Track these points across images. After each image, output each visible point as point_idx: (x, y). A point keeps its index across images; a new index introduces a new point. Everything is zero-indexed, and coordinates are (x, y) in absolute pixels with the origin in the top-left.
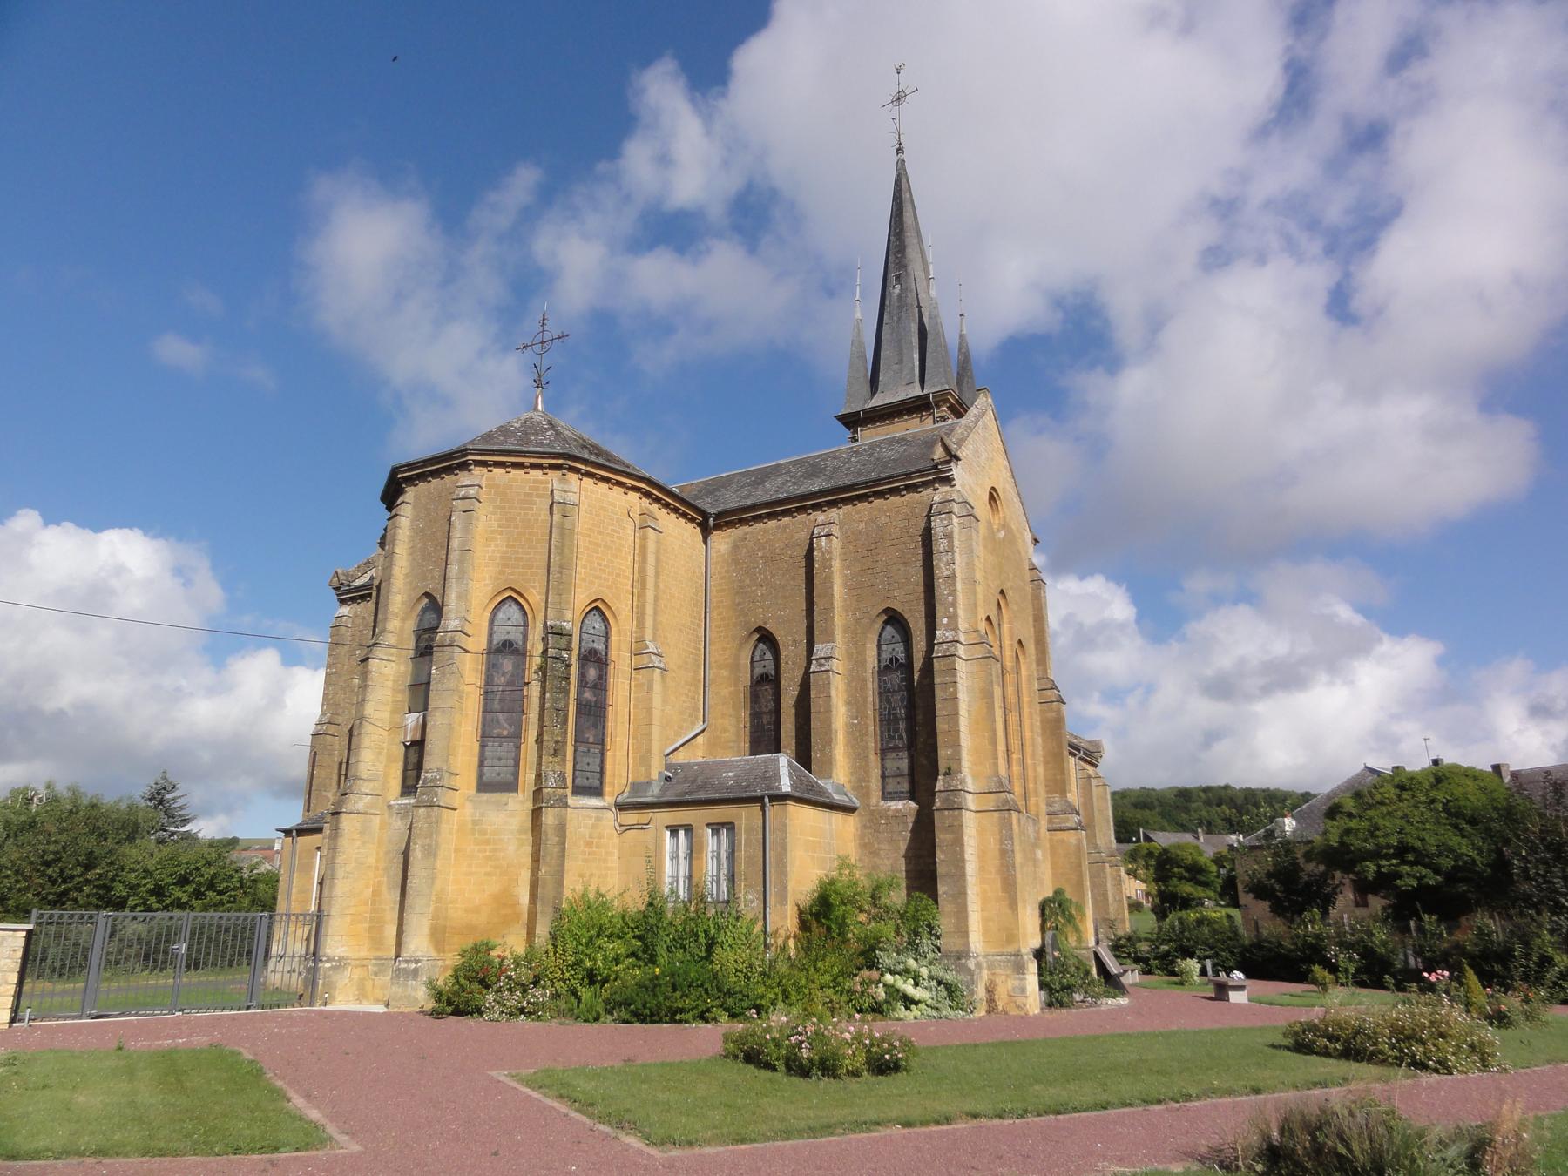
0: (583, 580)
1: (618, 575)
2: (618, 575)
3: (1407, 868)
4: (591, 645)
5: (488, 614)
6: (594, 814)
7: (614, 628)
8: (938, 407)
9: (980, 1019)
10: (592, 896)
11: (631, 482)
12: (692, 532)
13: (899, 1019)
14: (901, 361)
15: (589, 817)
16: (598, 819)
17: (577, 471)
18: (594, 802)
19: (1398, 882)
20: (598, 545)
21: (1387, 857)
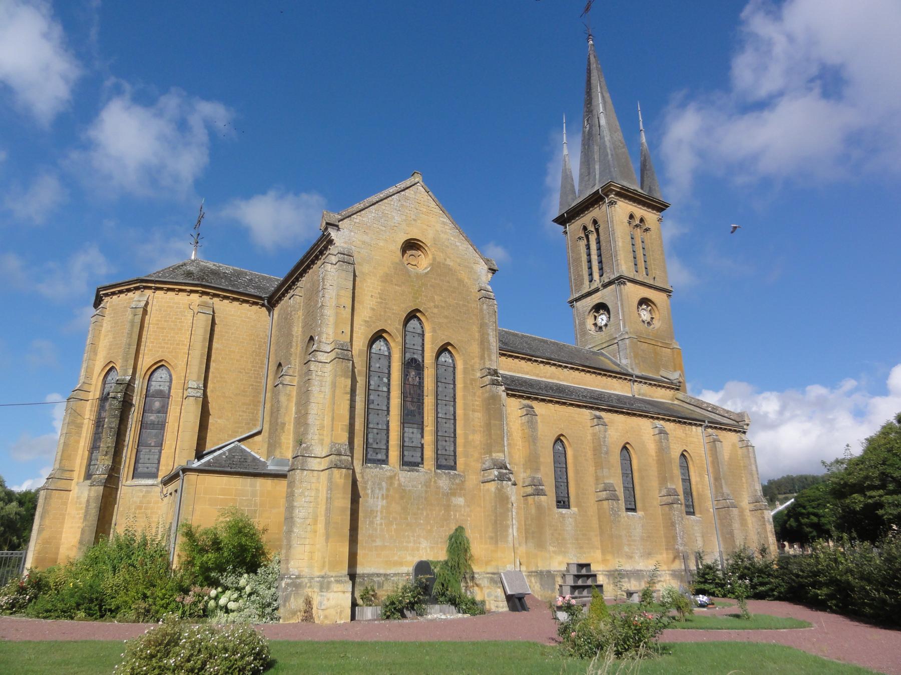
0: (151, 350)
1: (178, 344)
2: (178, 344)
3: (890, 498)
4: (158, 388)
5: (101, 378)
6: (144, 489)
7: (174, 377)
8: (607, 196)
9: (295, 625)
10: (122, 538)
11: (189, 288)
12: (253, 314)
13: (665, 649)
14: (589, 174)
15: (141, 491)
16: (147, 492)
17: (150, 288)
18: (150, 482)
19: (880, 512)
20: (163, 328)
21: (873, 488)
